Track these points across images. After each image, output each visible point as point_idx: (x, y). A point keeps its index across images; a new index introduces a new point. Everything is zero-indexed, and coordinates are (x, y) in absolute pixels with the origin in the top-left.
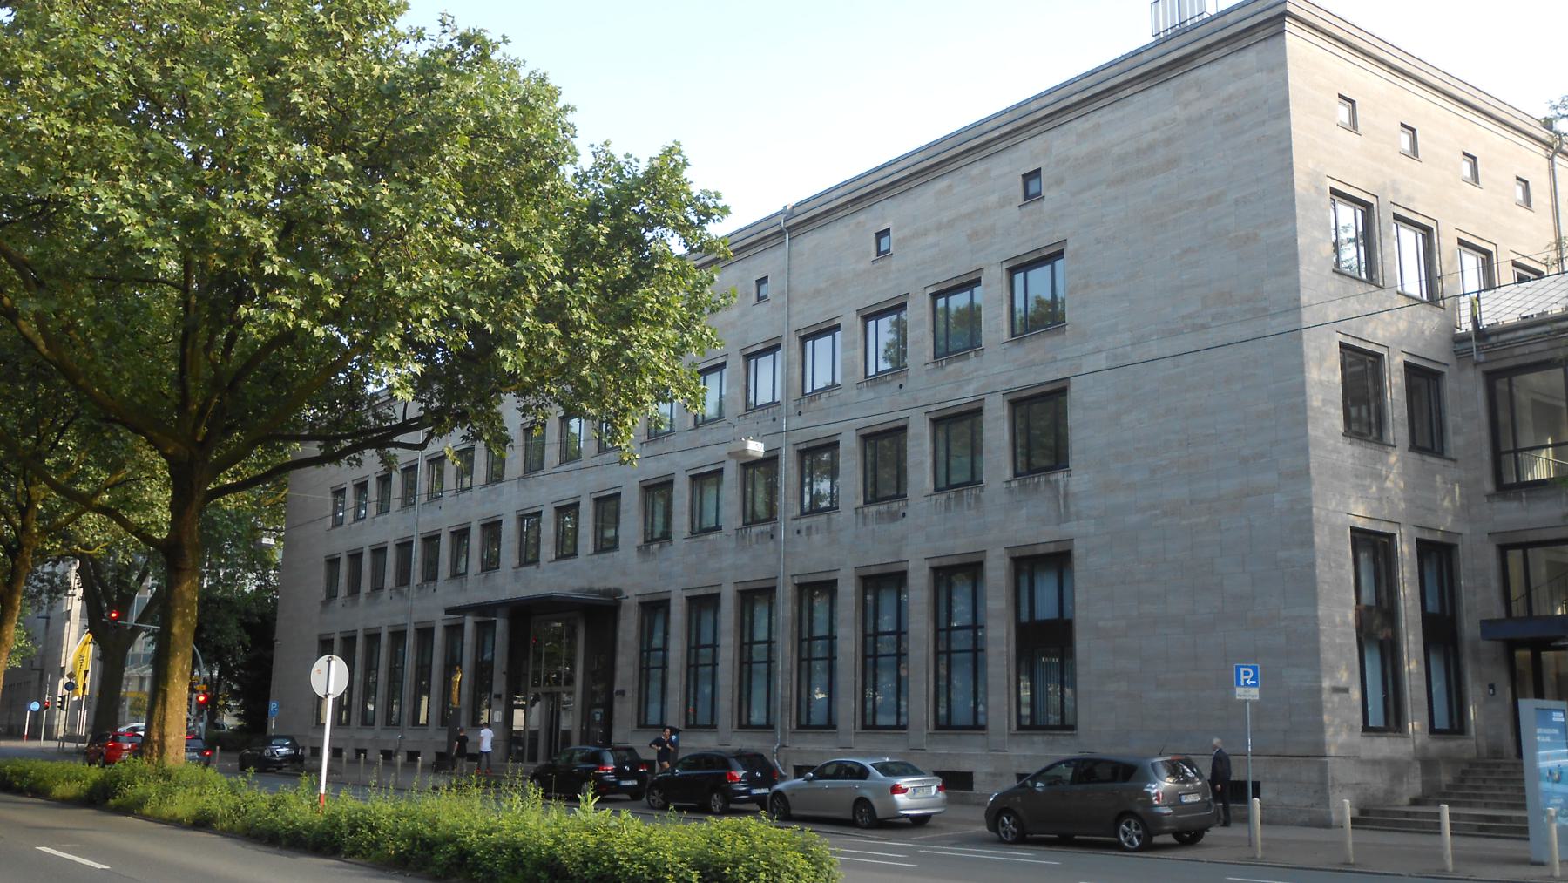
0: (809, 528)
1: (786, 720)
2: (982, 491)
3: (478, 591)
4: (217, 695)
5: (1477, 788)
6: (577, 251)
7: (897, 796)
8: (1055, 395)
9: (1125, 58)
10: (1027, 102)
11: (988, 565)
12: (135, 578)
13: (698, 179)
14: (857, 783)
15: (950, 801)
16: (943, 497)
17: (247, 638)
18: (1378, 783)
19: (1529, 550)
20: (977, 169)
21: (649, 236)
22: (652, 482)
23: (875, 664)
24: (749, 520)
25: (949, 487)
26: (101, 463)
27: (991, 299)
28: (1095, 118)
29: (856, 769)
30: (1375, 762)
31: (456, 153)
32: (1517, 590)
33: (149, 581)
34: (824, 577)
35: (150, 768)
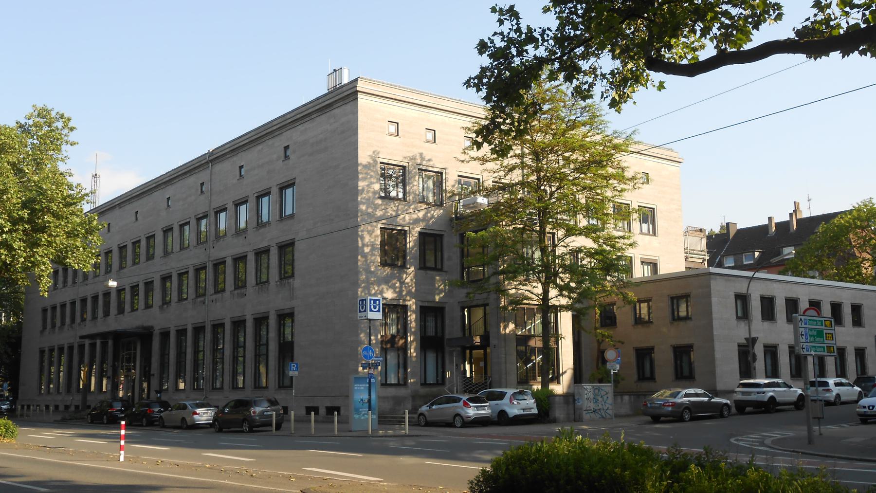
3: (102, 327)
8: (291, 244)
20: (270, 142)
22: (283, 244)
24: (237, 287)
25: (261, 283)
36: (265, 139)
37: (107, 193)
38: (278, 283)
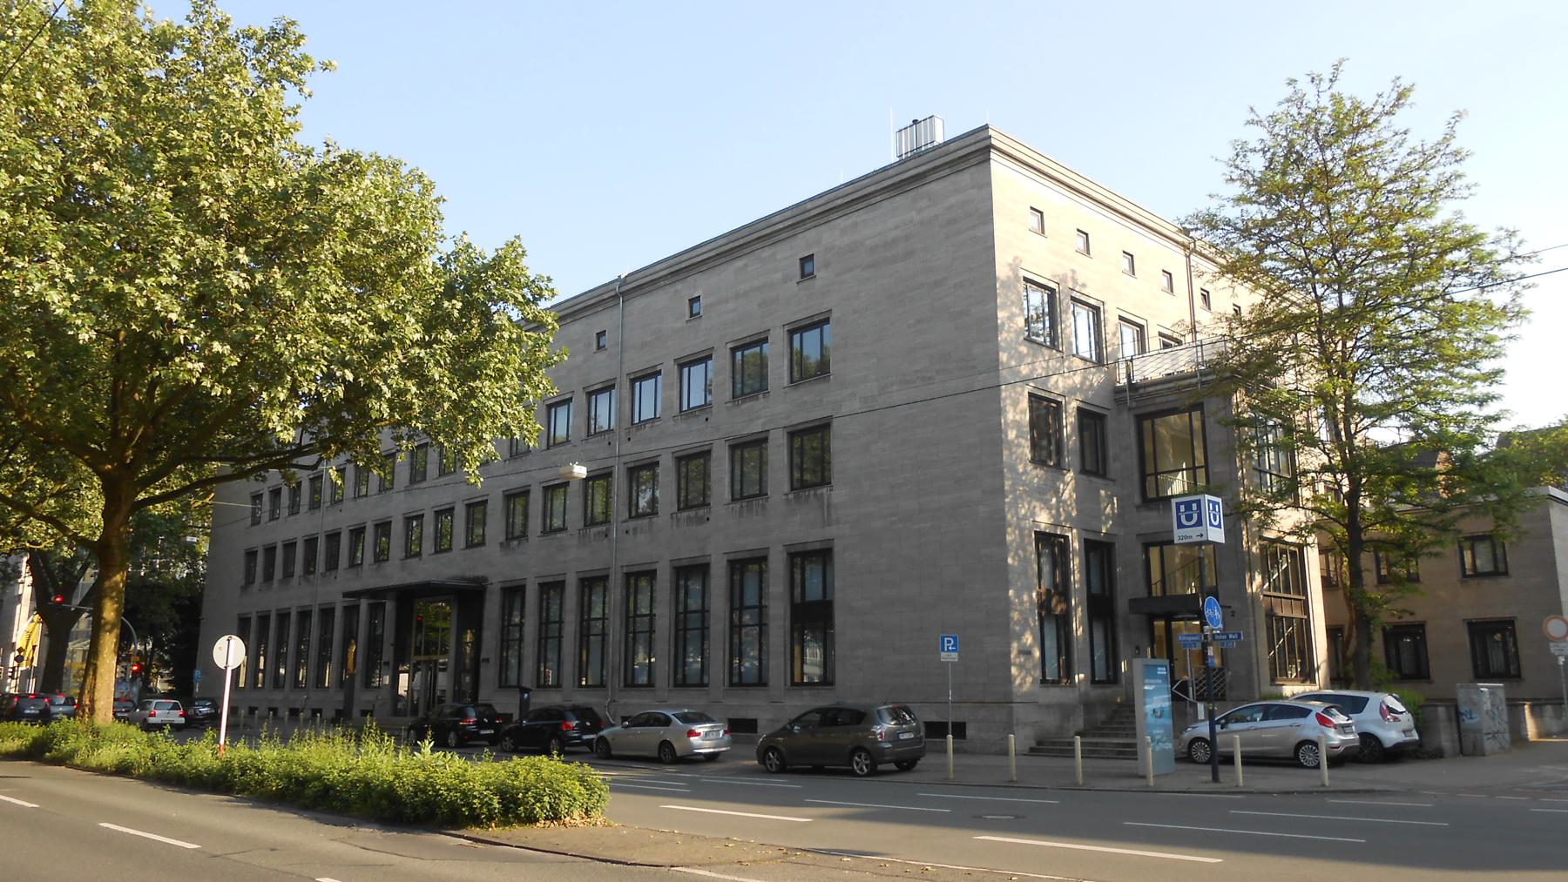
0: (635, 529)
1: (615, 681)
2: (767, 501)
3: (370, 578)
4: (151, 665)
5: (1122, 723)
6: (433, 322)
7: (692, 739)
8: (822, 428)
9: (876, 173)
10: (804, 202)
11: (771, 558)
12: (78, 567)
13: (532, 267)
14: (661, 730)
15: (734, 742)
16: (737, 506)
17: (177, 617)
18: (1051, 721)
19: (1165, 547)
20: (766, 253)
21: (494, 309)
22: (513, 492)
23: (634, 639)
25: (743, 498)
26: (48, 474)
27: (776, 354)
28: (854, 218)
29: (662, 718)
30: (1048, 706)
31: (331, 247)
32: (1156, 575)
33: (90, 571)
34: (646, 568)
35: (81, 727)
36: (754, 248)
37: (569, 285)
38: (791, 496)
